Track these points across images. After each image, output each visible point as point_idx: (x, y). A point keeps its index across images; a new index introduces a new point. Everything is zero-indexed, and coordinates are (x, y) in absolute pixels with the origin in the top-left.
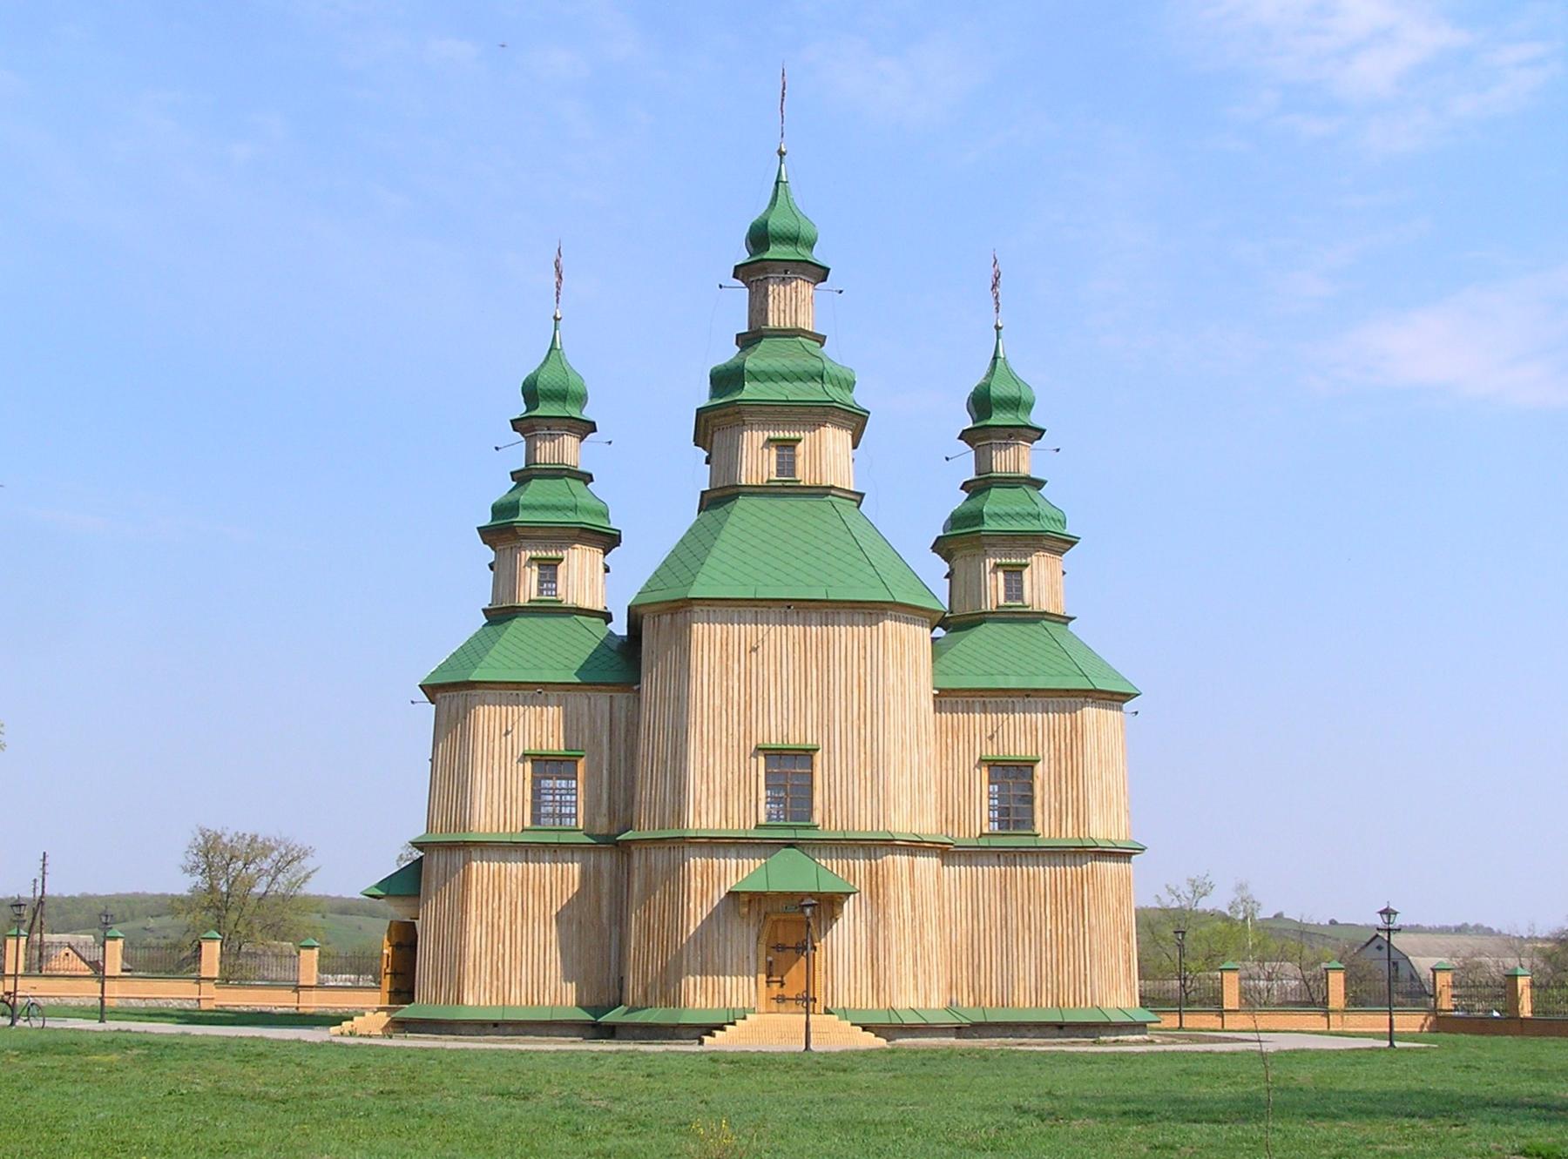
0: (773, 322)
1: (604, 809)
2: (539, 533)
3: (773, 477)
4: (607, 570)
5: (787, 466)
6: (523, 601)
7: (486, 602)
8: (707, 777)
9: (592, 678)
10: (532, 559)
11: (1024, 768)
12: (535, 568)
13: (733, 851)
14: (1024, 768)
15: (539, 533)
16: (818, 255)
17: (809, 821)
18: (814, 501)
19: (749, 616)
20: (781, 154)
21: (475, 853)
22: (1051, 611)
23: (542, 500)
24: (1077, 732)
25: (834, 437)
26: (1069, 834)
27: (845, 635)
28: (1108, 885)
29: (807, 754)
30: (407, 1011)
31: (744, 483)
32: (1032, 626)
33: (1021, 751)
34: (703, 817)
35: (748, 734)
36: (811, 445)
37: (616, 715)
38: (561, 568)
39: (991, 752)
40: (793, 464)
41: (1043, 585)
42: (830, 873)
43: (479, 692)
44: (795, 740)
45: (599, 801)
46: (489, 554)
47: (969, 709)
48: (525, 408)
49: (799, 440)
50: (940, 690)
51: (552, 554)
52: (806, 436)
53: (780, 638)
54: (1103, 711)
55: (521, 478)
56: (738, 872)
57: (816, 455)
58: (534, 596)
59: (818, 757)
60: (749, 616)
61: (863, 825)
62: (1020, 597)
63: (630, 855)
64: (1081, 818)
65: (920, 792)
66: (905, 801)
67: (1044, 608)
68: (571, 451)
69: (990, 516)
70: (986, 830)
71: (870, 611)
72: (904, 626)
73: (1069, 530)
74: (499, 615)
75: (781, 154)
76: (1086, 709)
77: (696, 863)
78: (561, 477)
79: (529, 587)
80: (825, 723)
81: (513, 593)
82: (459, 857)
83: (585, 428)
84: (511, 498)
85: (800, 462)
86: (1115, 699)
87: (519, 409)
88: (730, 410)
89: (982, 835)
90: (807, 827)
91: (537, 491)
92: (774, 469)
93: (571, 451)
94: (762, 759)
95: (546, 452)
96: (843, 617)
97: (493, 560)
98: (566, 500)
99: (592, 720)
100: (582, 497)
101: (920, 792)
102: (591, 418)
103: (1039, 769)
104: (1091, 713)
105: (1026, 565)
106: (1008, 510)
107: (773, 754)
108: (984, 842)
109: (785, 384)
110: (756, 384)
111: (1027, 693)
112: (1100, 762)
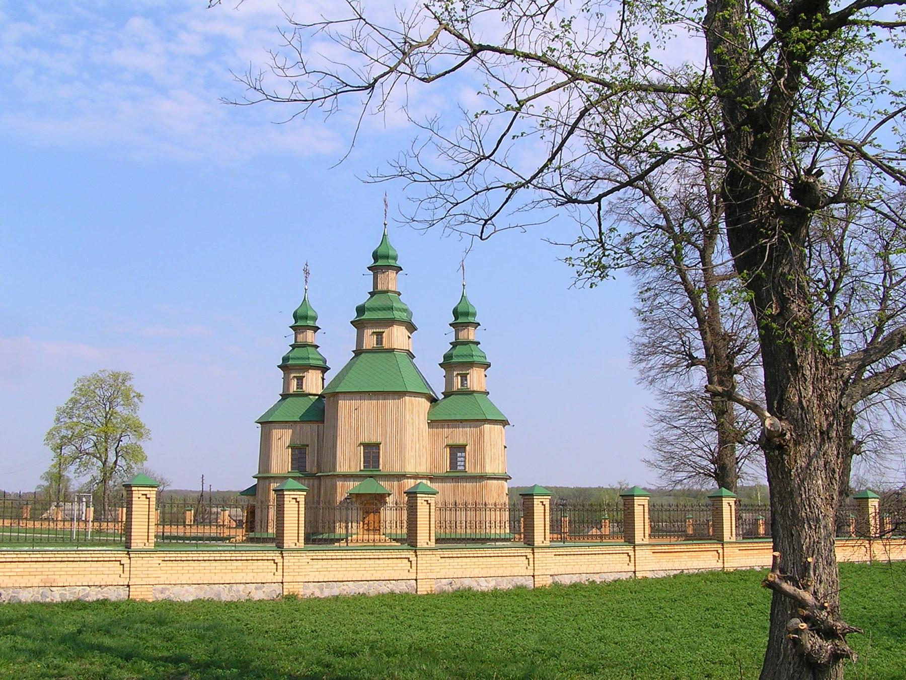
0: (380, 288)
1: (316, 464)
2: (296, 368)
3: (375, 346)
4: (486, 376)
5: (380, 341)
6: (291, 392)
7: (281, 392)
8: (343, 454)
9: (305, 419)
10: (294, 377)
11: (462, 448)
12: (296, 380)
13: (352, 479)
14: (462, 448)
15: (296, 368)
16: (399, 263)
17: (334, 471)
18: (388, 354)
19: (358, 397)
20: (385, 224)
21: (272, 480)
22: (478, 390)
23: (298, 356)
24: (482, 434)
25: (397, 330)
26: (478, 471)
27: (391, 403)
28: (493, 489)
29: (377, 445)
30: (252, 535)
31: (364, 348)
32: (470, 396)
33: (461, 442)
34: (343, 467)
35: (357, 439)
36: (389, 334)
37: (320, 431)
38: (304, 379)
39: (450, 442)
40: (382, 341)
41: (475, 380)
42: (385, 486)
43: (273, 424)
44: (373, 440)
45: (314, 461)
46: (443, 371)
47: (443, 427)
48: (454, 319)
49: (384, 332)
50: (431, 421)
51: (301, 375)
52: (386, 330)
53: (367, 405)
54: (492, 426)
55: (454, 345)
56: (352, 486)
57: (390, 337)
58: (295, 390)
59: (381, 445)
60: (358, 397)
61: (397, 469)
62: (302, 388)
63: (320, 480)
64: (483, 466)
65: (420, 458)
66: (413, 461)
67: (475, 389)
68: (310, 336)
69: (455, 356)
70: (448, 470)
71: (401, 394)
72: (413, 398)
73: (488, 360)
74: (285, 396)
75: (385, 224)
76: (485, 425)
77: (339, 484)
78: (305, 347)
79: (457, 383)
80: (384, 435)
81: (288, 388)
82: (267, 481)
83: (316, 329)
84: (450, 352)
85: (384, 340)
86: (504, 423)
87: (292, 322)
88: (360, 322)
89: (447, 472)
90: (377, 471)
91: (460, 350)
92: (375, 343)
93: (310, 336)
94: (362, 447)
95: (463, 335)
96: (391, 397)
97: (444, 374)
98: (305, 355)
99: (311, 434)
100: (313, 354)
101: (420, 458)
102: (478, 321)
103: (467, 448)
104: (487, 427)
105: (468, 374)
106: (461, 353)
107: (366, 446)
108: (446, 475)
109: (380, 312)
110: (369, 312)
111: (461, 421)
112: (491, 445)
